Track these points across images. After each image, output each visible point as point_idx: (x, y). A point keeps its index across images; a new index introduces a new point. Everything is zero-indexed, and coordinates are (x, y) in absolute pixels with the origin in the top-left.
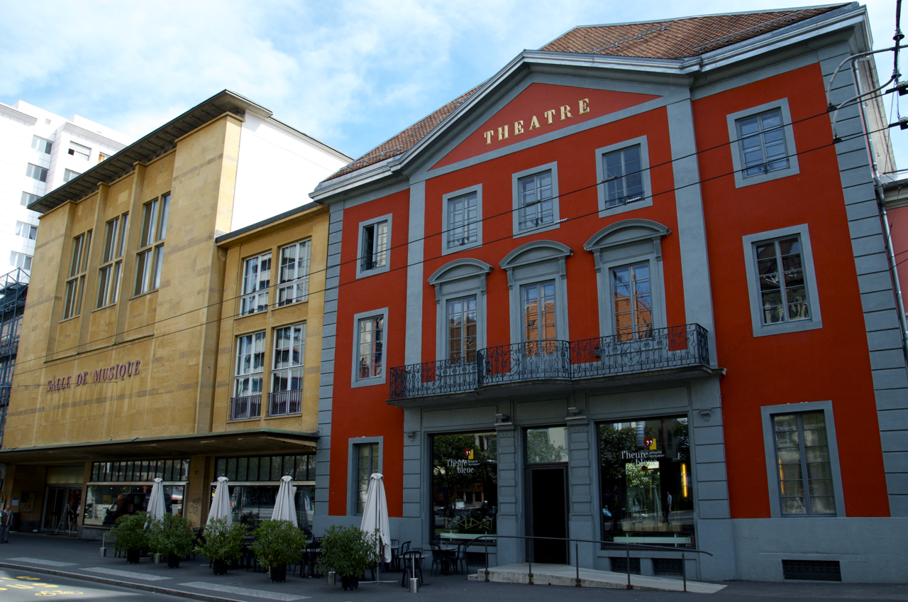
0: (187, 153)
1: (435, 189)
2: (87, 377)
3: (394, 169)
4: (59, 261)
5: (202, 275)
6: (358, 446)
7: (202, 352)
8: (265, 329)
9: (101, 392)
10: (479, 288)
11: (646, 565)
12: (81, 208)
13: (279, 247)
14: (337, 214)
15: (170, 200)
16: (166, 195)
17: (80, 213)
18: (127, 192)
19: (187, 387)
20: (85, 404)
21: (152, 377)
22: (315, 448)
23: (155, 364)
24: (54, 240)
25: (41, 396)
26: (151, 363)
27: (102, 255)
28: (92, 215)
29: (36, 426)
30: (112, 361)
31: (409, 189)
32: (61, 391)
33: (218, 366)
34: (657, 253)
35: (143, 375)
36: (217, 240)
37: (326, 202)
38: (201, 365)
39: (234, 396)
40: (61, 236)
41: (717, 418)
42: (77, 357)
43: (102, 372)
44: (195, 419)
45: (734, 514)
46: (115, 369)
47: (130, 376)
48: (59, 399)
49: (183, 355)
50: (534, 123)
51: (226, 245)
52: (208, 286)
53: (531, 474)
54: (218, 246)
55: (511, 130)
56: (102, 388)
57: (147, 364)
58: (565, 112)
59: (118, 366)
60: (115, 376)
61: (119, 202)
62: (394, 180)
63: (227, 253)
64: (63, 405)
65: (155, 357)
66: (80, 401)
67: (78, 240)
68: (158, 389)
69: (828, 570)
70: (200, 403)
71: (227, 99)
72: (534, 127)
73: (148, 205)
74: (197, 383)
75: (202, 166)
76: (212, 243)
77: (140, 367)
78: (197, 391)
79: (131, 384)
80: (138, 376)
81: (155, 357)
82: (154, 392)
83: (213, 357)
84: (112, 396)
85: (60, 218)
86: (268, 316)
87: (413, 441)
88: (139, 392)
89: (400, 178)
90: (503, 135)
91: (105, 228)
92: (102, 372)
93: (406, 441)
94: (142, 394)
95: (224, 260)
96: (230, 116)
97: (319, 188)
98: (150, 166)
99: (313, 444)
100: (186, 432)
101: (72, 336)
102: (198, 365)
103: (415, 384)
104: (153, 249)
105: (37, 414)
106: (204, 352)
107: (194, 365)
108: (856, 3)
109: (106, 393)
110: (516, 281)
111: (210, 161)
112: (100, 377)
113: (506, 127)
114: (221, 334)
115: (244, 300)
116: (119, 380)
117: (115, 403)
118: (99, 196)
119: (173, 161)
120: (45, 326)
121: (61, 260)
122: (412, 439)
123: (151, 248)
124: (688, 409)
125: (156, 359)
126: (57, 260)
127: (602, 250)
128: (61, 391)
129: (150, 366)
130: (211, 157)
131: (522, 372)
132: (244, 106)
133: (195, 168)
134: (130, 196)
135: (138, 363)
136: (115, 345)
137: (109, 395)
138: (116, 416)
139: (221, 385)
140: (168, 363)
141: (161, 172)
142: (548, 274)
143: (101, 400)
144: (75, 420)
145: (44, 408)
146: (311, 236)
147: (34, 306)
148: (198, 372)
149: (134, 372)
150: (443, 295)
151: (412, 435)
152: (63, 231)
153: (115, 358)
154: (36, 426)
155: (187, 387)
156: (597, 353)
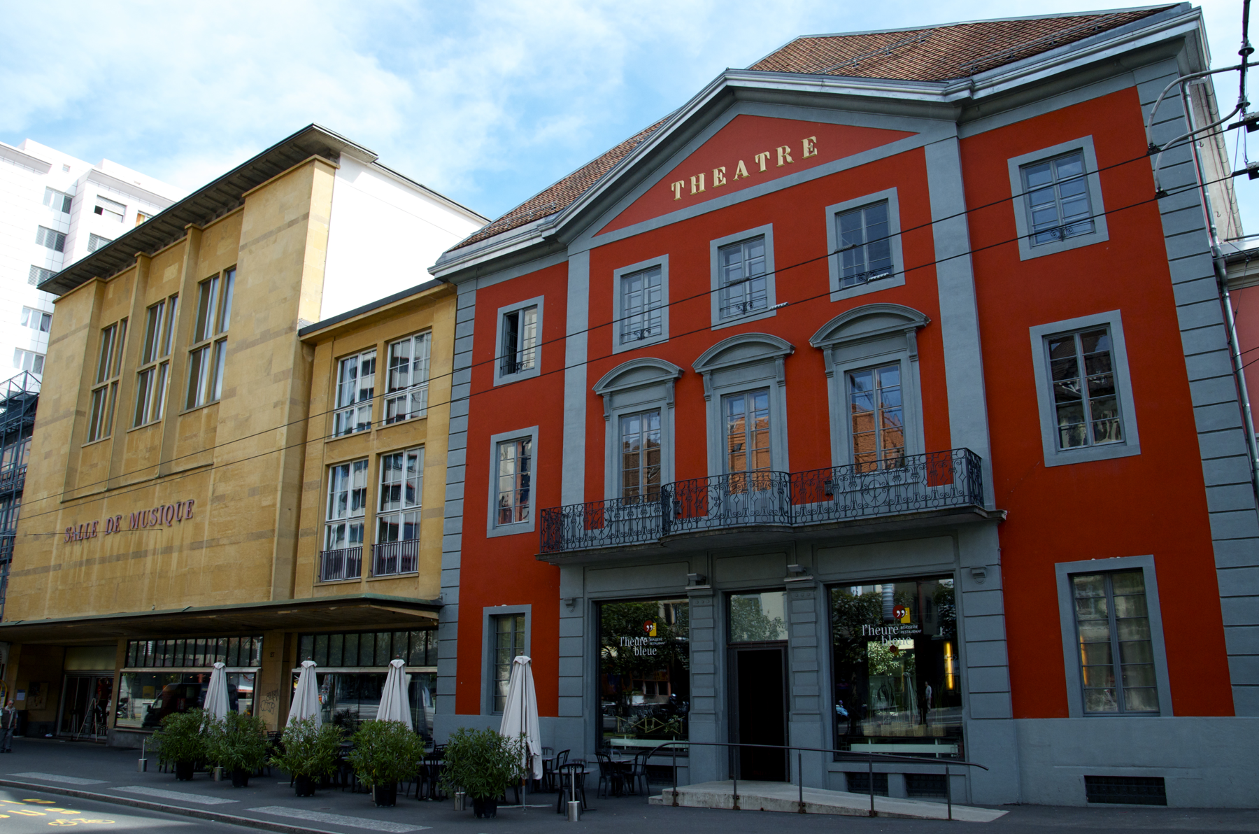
1: (603, 261)
2: (121, 522)
3: (546, 234)
4: (81, 361)
5: (280, 380)
7: (280, 488)
8: (368, 456)
9: (139, 543)
10: (664, 399)
12: (111, 287)
13: (387, 342)
14: (467, 296)
16: (230, 271)
17: (110, 296)
18: (176, 265)
19: (259, 536)
21: (211, 523)
22: (437, 620)
23: (215, 505)
25: (57, 549)
26: (209, 503)
29: (49, 591)
31: (568, 261)
33: (303, 507)
34: (911, 351)
36: (301, 333)
38: (278, 505)
39: (325, 549)
40: (85, 327)
44: (270, 580)
47: (180, 521)
48: (82, 553)
49: (253, 492)
52: (288, 396)
55: (709, 180)
56: (141, 538)
57: (203, 504)
58: (783, 155)
60: (159, 521)
61: (165, 280)
62: (546, 249)
63: (314, 350)
64: (88, 561)
65: (216, 494)
68: (218, 540)
71: (315, 137)
75: (280, 229)
77: (194, 508)
78: (273, 542)
80: (191, 521)
82: (213, 543)
83: (296, 495)
86: (371, 437)
87: (572, 611)
93: (564, 611)
94: (196, 546)
96: (318, 160)
98: (208, 230)
99: (434, 615)
102: (274, 505)
103: (575, 532)
105: (51, 573)
106: (283, 487)
108: (1187, 4)
112: (138, 522)
113: (702, 176)
115: (338, 416)
116: (165, 527)
118: (137, 271)
119: (240, 224)
122: (571, 609)
125: (217, 497)
126: (79, 360)
127: (835, 347)
129: (209, 507)
130: (293, 217)
133: (271, 233)
134: (180, 271)
135: (191, 503)
136: (159, 478)
137: (151, 547)
139: (306, 534)
140: (232, 503)
142: (760, 380)
143: (139, 554)
144: (103, 582)
145: (60, 565)
146: (430, 327)
147: (47, 423)
148: (275, 516)
149: (185, 516)
151: (571, 602)
152: (87, 320)
153: (160, 496)
154: (49, 591)
155: (259, 536)
156: (827, 489)
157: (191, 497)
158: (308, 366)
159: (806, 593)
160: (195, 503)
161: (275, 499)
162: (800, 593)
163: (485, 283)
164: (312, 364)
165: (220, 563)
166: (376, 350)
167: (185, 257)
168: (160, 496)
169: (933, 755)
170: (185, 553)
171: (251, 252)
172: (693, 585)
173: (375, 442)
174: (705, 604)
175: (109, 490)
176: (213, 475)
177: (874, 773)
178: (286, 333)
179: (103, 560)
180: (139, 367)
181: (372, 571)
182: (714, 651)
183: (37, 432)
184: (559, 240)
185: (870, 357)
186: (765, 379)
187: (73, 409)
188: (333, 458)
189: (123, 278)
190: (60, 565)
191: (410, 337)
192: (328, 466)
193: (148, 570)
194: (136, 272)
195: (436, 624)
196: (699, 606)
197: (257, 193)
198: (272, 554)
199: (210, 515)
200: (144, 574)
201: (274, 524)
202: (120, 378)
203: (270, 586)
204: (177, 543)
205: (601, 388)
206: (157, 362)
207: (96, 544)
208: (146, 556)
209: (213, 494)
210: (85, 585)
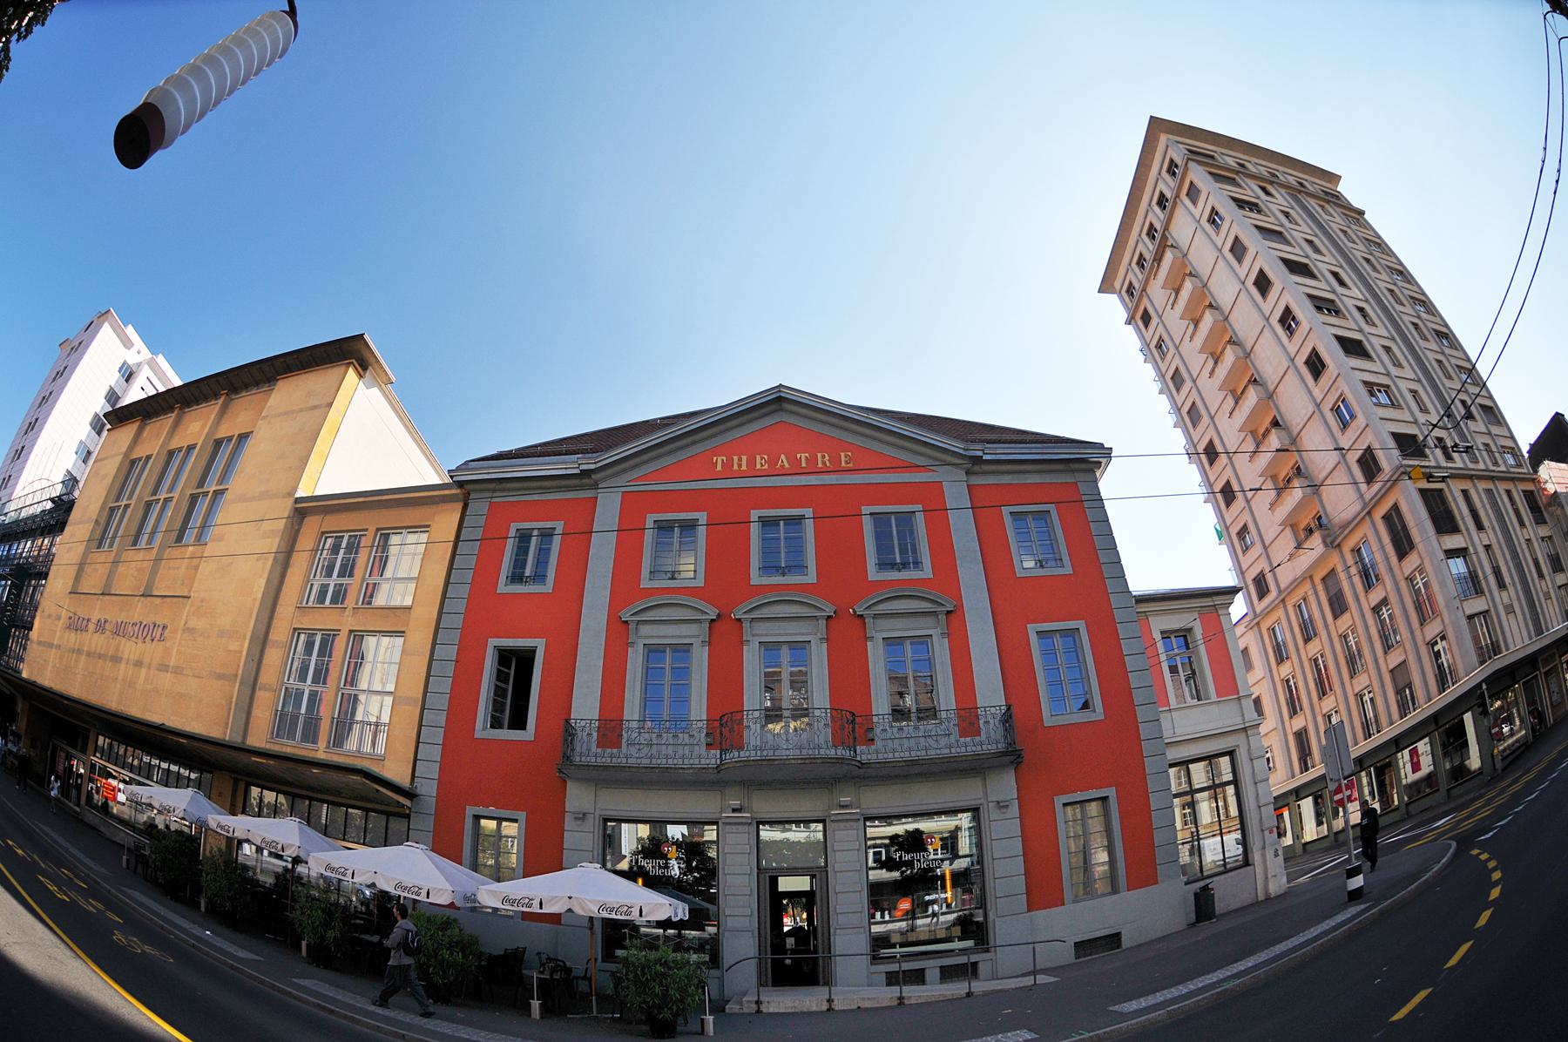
0: (288, 393)
2: (107, 625)
4: (110, 481)
5: (268, 538)
6: (766, 522)
7: (248, 637)
8: (339, 630)
9: (117, 649)
10: (698, 637)
11: (933, 974)
12: (148, 428)
13: (378, 530)
15: (251, 441)
16: (244, 437)
17: (145, 435)
18: (201, 423)
19: (221, 677)
20: (100, 658)
21: (179, 652)
22: (410, 809)
23: (184, 635)
24: (113, 456)
25: (60, 631)
26: (180, 632)
27: (150, 488)
28: (156, 437)
29: (51, 664)
30: (136, 615)
32: (79, 632)
33: (264, 662)
34: (942, 629)
35: (168, 644)
36: (298, 500)
37: (468, 487)
38: (244, 653)
40: (121, 454)
41: (1014, 810)
42: (101, 597)
43: (123, 625)
44: (227, 724)
45: (1032, 906)
46: (138, 625)
47: (153, 640)
48: (76, 642)
49: (222, 634)
50: (782, 461)
51: (304, 510)
53: (769, 965)
54: (296, 509)
56: (119, 645)
57: (175, 632)
58: (823, 459)
59: (141, 623)
60: (135, 635)
61: (189, 432)
63: (302, 521)
64: (78, 650)
65: (187, 626)
66: (95, 653)
67: (131, 465)
68: (183, 668)
69: (1113, 940)
70: (236, 704)
71: (360, 346)
72: (782, 466)
73: (218, 443)
74: (236, 675)
75: (301, 410)
76: (290, 502)
77: (167, 632)
78: (234, 687)
79: (152, 651)
80: (162, 643)
81: (187, 626)
82: (178, 670)
83: (259, 649)
84: (128, 660)
85: (127, 433)
86: (346, 613)
87: (579, 826)
88: (160, 665)
89: (585, 481)
90: (740, 466)
91: (163, 458)
92: (123, 625)
93: (569, 823)
94: (163, 668)
95: (297, 527)
96: (354, 366)
97: (463, 467)
98: (236, 401)
100: (215, 732)
101: (100, 572)
102: (241, 652)
103: (588, 748)
104: (210, 494)
105: (54, 650)
106: (251, 637)
107: (235, 651)
108: (1102, 444)
109: (123, 653)
110: (753, 636)
111: (314, 408)
112: (119, 630)
114: (275, 621)
115: (312, 585)
116: (140, 641)
117: (131, 668)
118: (172, 419)
119: (267, 401)
120: (79, 551)
121: (113, 480)
122: (579, 822)
123: (209, 492)
124: (982, 801)
125: (188, 629)
126: (109, 480)
127: (875, 616)
128: (79, 632)
129: (179, 636)
130: (316, 403)
131: (761, 747)
132: (371, 360)
133: (293, 412)
134: (203, 427)
135: (164, 627)
136: (142, 595)
137: (126, 656)
138: (129, 686)
139: (264, 688)
140: (201, 639)
141: (246, 409)
142: (803, 634)
143: (116, 659)
144: (86, 673)
145: (60, 646)
146: (429, 526)
147: (75, 524)
148: (240, 662)
149: (158, 637)
150: (641, 637)
151: (581, 816)
152: (124, 449)
153: (140, 612)
154: (51, 664)
155: (221, 677)
156: (870, 736)
157: (165, 621)
158: (293, 533)
159: (848, 824)
160: (169, 628)
161: (243, 646)
162: (842, 825)
163: (383, 532)
164: (298, 532)
165: (182, 691)
166: (427, 531)
167: (213, 416)
168: (140, 612)
169: (952, 951)
170: (152, 672)
171: (269, 422)
172: (729, 813)
173: (350, 619)
174: (740, 831)
175: (102, 594)
176: (188, 607)
177: (904, 971)
178: (284, 497)
179: (89, 654)
180: (148, 497)
181: (329, 742)
182: (749, 875)
183: (68, 529)
184: (593, 477)
185: (909, 630)
186: (807, 634)
187: (95, 517)
188: (302, 623)
189: (158, 424)
190: (60, 646)
191: (403, 531)
192: (295, 629)
193: (120, 677)
194: (167, 421)
195: (407, 812)
196: (732, 833)
197: (290, 379)
198: (232, 698)
199: (180, 643)
200: (116, 679)
201: (237, 670)
202: (133, 502)
203: (227, 728)
204: (147, 660)
205: (627, 615)
206: (162, 496)
207: (86, 637)
208: (120, 662)
209: (185, 625)
210: (73, 671)
